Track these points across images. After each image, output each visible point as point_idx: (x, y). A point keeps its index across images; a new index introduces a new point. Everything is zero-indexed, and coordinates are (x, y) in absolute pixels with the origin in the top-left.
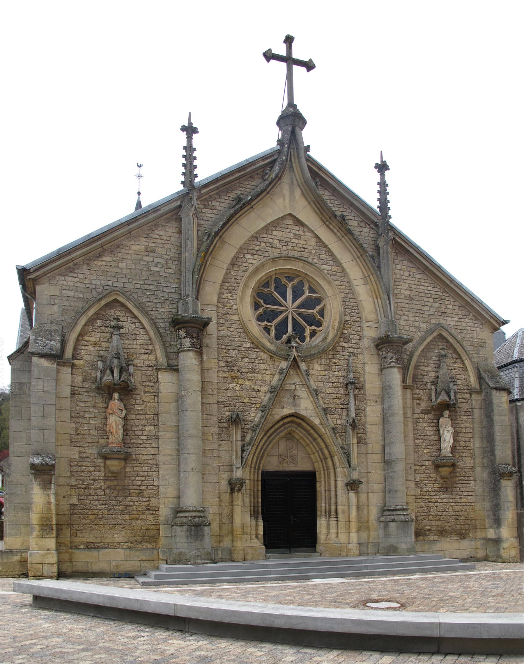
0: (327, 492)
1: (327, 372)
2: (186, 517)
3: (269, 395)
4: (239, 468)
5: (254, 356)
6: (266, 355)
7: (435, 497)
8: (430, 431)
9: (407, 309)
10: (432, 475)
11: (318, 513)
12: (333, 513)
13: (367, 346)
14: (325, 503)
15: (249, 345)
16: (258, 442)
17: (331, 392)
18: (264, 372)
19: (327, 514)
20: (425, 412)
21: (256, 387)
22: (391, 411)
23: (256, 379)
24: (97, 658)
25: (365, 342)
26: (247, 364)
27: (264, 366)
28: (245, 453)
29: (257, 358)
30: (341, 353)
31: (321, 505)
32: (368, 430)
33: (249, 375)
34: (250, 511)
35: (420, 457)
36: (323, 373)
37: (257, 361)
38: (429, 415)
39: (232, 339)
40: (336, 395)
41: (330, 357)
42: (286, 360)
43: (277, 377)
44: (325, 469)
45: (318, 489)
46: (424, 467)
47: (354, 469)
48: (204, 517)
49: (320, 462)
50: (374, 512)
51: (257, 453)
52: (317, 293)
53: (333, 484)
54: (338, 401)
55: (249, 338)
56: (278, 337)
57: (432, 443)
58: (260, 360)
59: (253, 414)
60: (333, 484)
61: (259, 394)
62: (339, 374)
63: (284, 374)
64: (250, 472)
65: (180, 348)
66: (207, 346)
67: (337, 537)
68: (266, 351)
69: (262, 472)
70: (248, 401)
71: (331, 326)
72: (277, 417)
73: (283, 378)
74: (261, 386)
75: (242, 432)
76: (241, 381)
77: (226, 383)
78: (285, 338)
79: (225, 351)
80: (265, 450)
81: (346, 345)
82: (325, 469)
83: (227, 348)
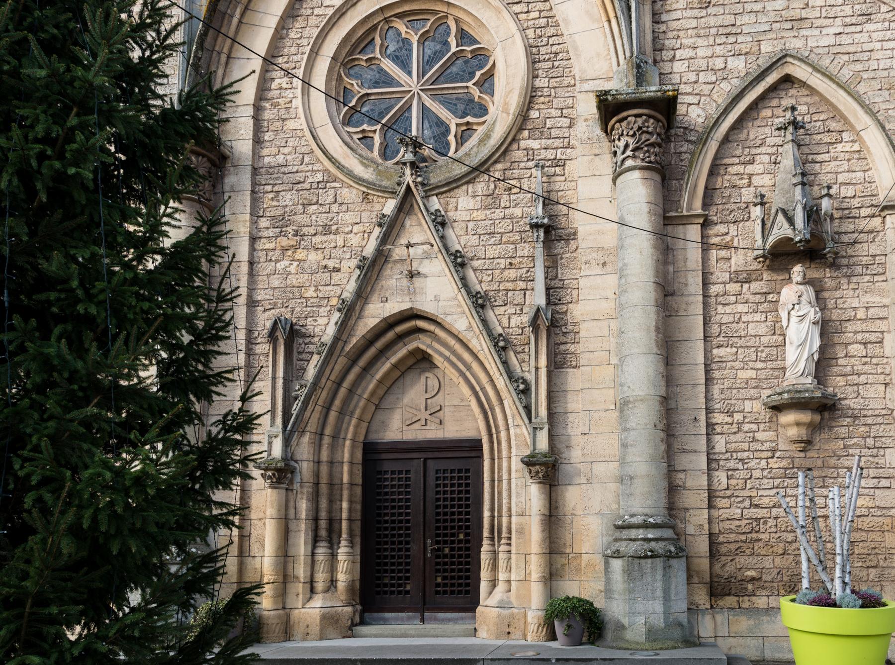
1: (488, 212)
4: (276, 436)
21: (331, 264)
33: (318, 239)
36: (480, 215)
37: (335, 208)
39: (286, 170)
54: (512, 273)
59: (322, 321)
61: (336, 277)
70: (314, 295)
76: (301, 254)
79: (271, 195)
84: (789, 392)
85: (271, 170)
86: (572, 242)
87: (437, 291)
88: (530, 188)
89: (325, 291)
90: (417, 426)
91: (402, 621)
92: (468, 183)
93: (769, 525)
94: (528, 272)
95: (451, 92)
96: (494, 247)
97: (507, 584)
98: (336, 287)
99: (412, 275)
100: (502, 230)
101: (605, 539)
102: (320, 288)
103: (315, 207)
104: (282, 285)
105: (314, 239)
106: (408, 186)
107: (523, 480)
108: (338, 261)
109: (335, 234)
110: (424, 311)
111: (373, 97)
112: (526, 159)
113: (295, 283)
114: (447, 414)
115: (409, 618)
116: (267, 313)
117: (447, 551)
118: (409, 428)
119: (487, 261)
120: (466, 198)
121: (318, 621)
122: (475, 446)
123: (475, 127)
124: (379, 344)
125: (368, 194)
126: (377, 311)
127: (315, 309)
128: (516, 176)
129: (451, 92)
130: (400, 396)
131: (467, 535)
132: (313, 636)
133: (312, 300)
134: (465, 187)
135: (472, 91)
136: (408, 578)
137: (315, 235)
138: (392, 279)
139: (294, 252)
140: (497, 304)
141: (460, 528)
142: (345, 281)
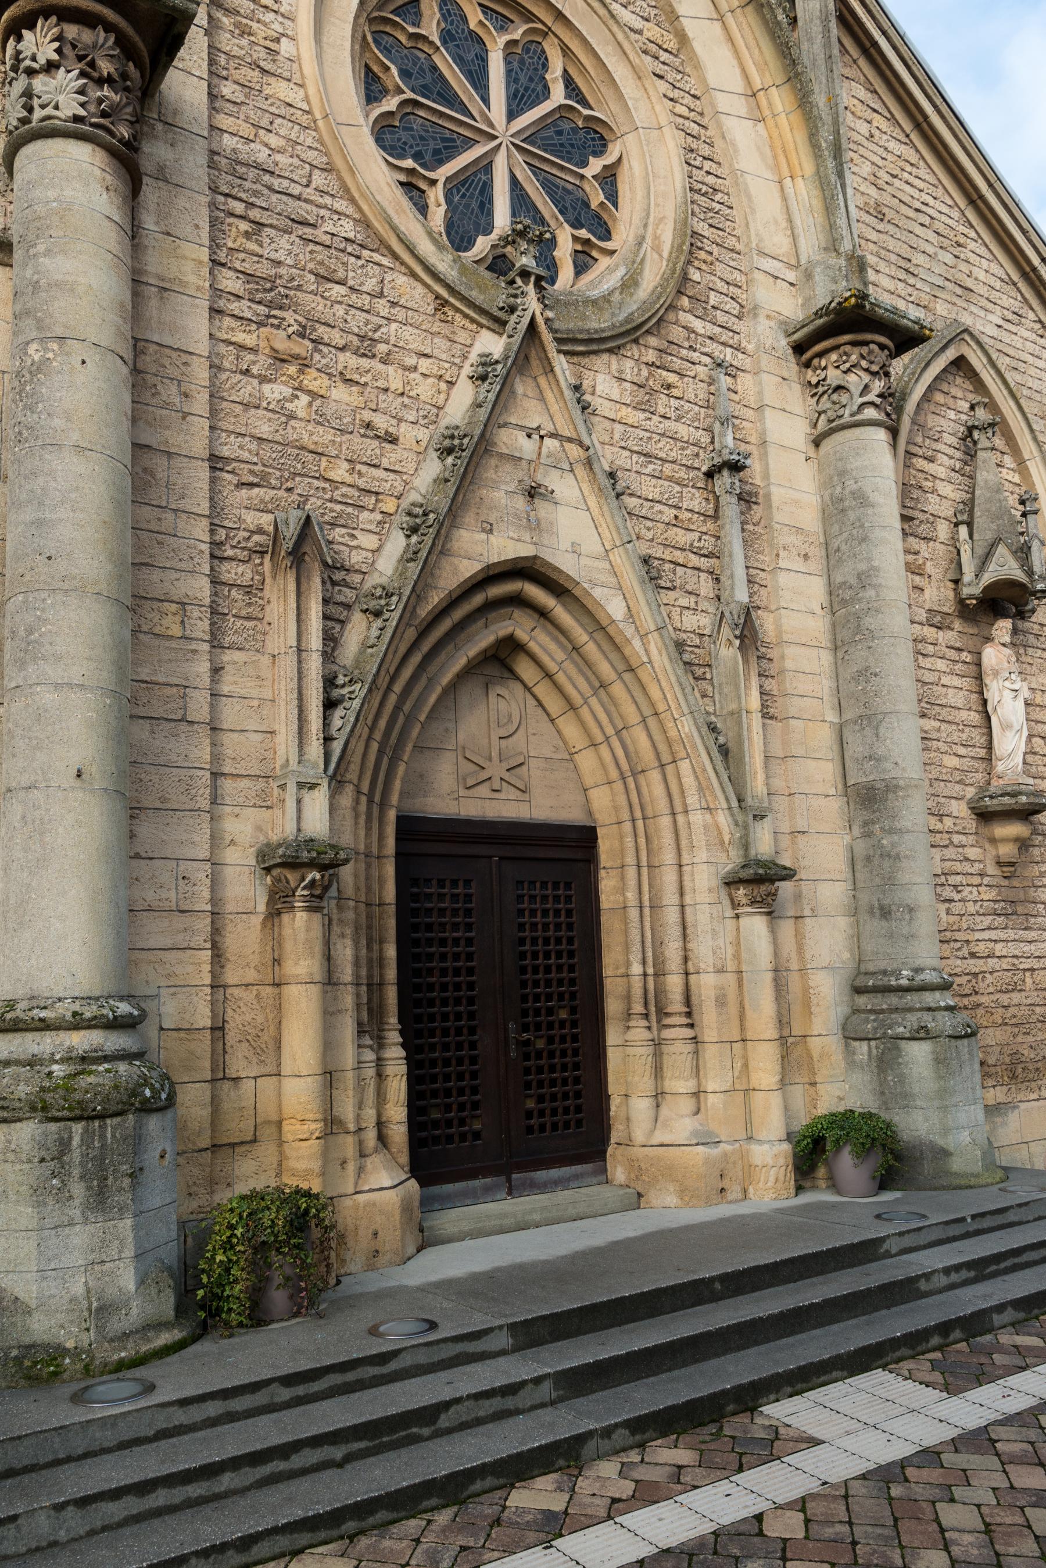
2: (32, 1062)
3: (433, 467)
4: (313, 786)
5: (370, 284)
6: (420, 289)
7: (986, 935)
8: (956, 692)
9: (871, 246)
10: (973, 853)
11: (613, 1006)
12: (676, 1004)
13: (768, 344)
14: (644, 963)
15: (348, 228)
17: (666, 492)
19: (652, 1008)
20: (937, 621)
21: (381, 422)
22: (871, 593)
25: (760, 328)
26: (340, 310)
27: (411, 338)
28: (339, 712)
29: (381, 295)
30: (684, 352)
31: (622, 965)
33: (349, 360)
35: (936, 784)
37: (382, 307)
38: (950, 634)
39: (276, 183)
40: (674, 511)
41: (651, 356)
42: (499, 324)
44: (638, 814)
45: (607, 899)
46: (948, 822)
47: (759, 817)
48: (140, 1055)
49: (619, 786)
50: (827, 995)
51: (382, 723)
52: (592, 109)
53: (669, 878)
54: (682, 537)
55: (352, 200)
56: (459, 236)
57: (964, 736)
58: (394, 304)
59: (369, 541)
60: (669, 878)
61: (391, 456)
62: (683, 431)
63: (499, 381)
65: (24, 121)
66: (162, 175)
67: (697, 1112)
68: (419, 270)
69: (401, 820)
70: (349, 479)
71: (649, 240)
72: (468, 569)
73: (491, 396)
74: (400, 420)
75: (326, 601)
76: (314, 381)
77: (247, 372)
78: (482, 245)
79: (244, 226)
80: (410, 719)
81: (698, 325)
82: (638, 814)
83: (255, 214)
84: (1027, 795)
85: (241, 170)
87: (576, 535)
90: (483, 790)
92: (610, 351)
93: (987, 982)
95: (554, 171)
97: (693, 1100)
98: (392, 476)
99: (533, 493)
101: (839, 1009)
102: (358, 467)
103: (342, 290)
106: (532, 324)
111: (421, 113)
112: (686, 344)
115: (487, 1190)
116: (244, 492)
117: (540, 1044)
118: (470, 793)
122: (584, 839)
123: (594, 254)
124: (458, 614)
125: (445, 303)
126: (477, 548)
127: (350, 510)
129: (554, 171)
130: (451, 725)
131: (573, 1010)
132: (388, 1257)
135: (587, 188)
139: (301, 372)
140: (663, 584)
141: (561, 997)
142: (410, 468)
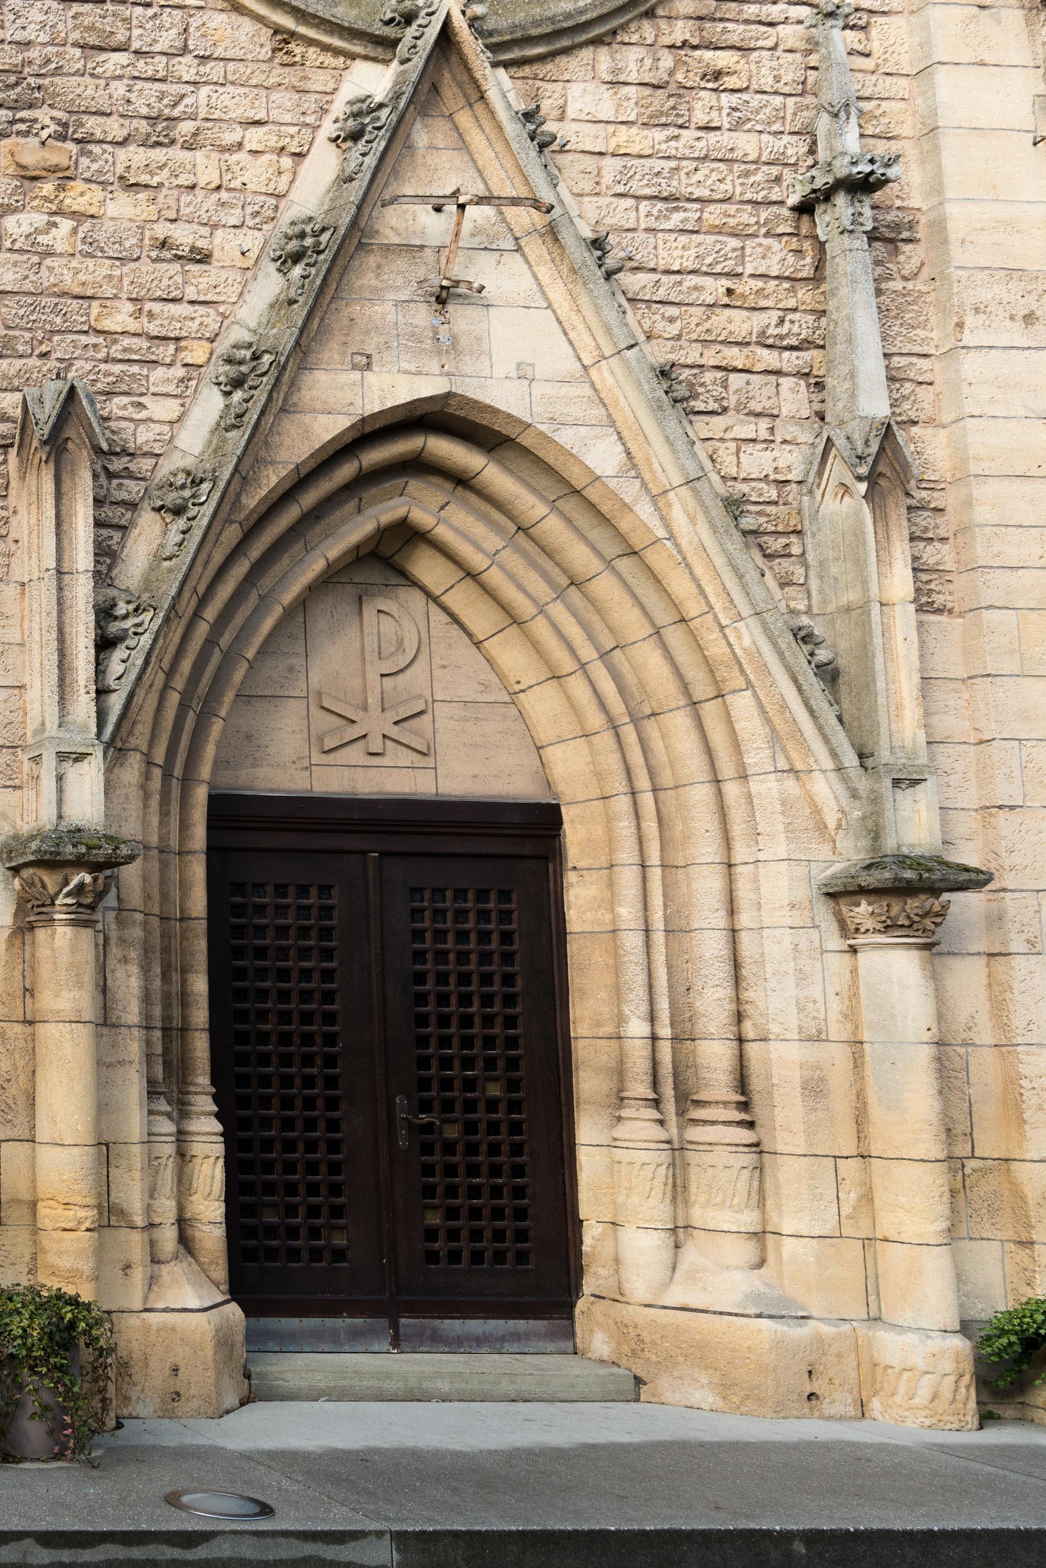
0: (659, 938)
1: (659, 135)
3: (270, 284)
4: (80, 757)
5: (167, 40)
11: (588, 1084)
14: (652, 1018)
16: (201, 589)
18: (230, 137)
19: (668, 1091)
21: (184, 236)
23: (182, 180)
24: (172, 318)
26: (119, 89)
27: (235, 103)
28: (119, 653)
29: (185, 50)
32: (982, 513)
33: (135, 156)
34: (149, 1057)
36: (639, 140)
37: (186, 68)
40: (726, 283)
43: (324, 164)
44: (643, 782)
49: (606, 740)
51: (186, 666)
53: (706, 887)
54: (740, 323)
58: (203, 59)
59: (164, 409)
60: (706, 887)
61: (200, 281)
62: (747, 144)
63: (381, 139)
64: (144, 787)
70: (133, 326)
72: (327, 427)
73: (371, 161)
74: (215, 227)
76: (80, 197)
80: (230, 657)
82: (643, 782)
86: (907, 248)
87: (527, 350)
88: (777, 79)
89: (169, 318)
90: (354, 754)
91: (336, 1343)
92: (597, 42)
94: (781, 321)
96: (683, 239)
98: (201, 310)
100: (705, 193)
102: (148, 306)
104: (28, 286)
105: (122, 154)
107: (814, 934)
108: (205, 231)
109: (188, 147)
110: (476, 404)
113: (69, 282)
114: (445, 725)
115: (356, 1335)
118: (331, 758)
119: (665, 279)
120: (591, 86)
121: (209, 1352)
124: (310, 498)
126: (340, 397)
127: (135, 369)
128: (734, 39)
130: (298, 662)
131: (513, 1085)
132: (195, 1404)
133: (126, 341)
134: (586, 54)
136: (337, 1212)
137: (123, 143)
138: (385, 299)
139: (61, 188)
